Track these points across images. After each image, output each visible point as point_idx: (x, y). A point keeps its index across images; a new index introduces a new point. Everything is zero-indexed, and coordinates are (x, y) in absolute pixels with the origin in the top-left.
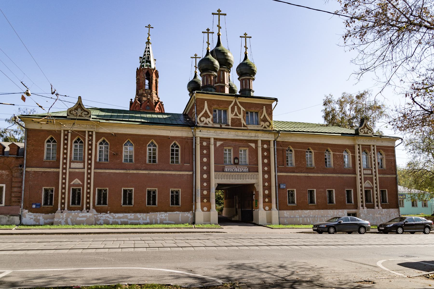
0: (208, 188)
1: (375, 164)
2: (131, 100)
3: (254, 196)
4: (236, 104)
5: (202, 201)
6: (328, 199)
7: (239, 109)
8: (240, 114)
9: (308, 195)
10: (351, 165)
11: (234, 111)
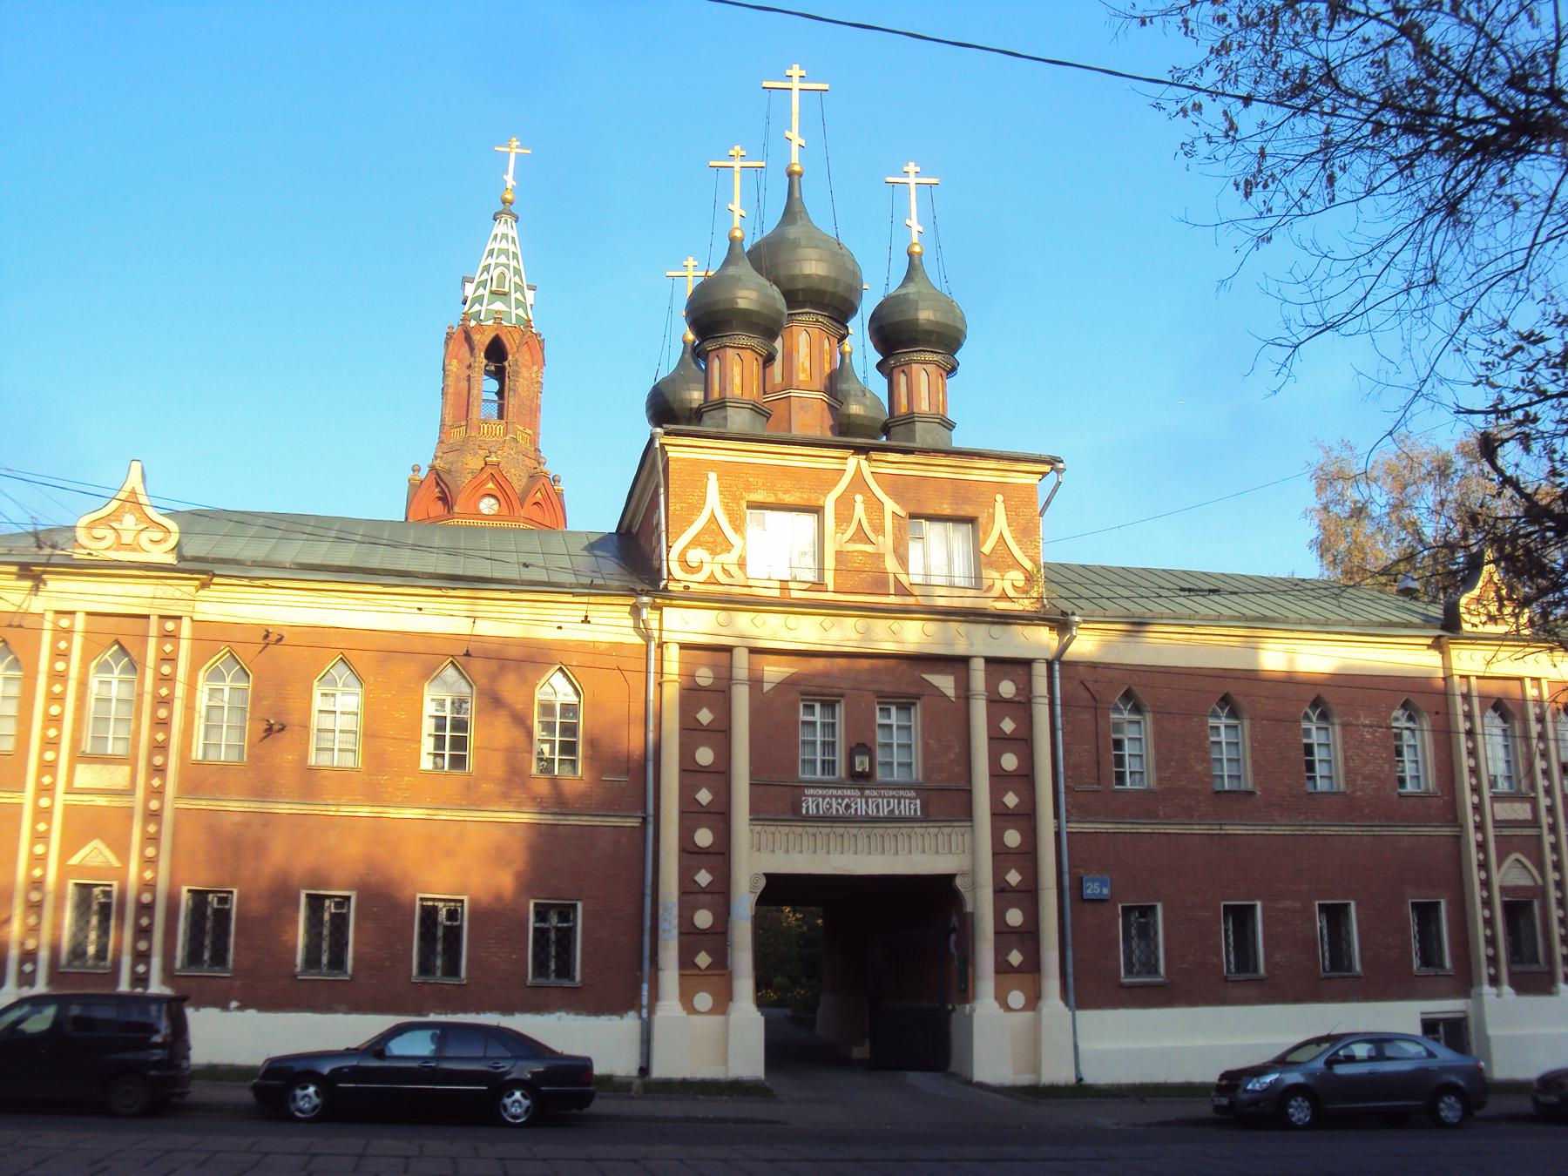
0: (721, 895)
1: (1546, 773)
2: (416, 469)
3: (953, 937)
4: (858, 482)
5: (686, 962)
6: (1324, 953)
7: (875, 506)
8: (879, 530)
9: (1224, 933)
11: (849, 520)
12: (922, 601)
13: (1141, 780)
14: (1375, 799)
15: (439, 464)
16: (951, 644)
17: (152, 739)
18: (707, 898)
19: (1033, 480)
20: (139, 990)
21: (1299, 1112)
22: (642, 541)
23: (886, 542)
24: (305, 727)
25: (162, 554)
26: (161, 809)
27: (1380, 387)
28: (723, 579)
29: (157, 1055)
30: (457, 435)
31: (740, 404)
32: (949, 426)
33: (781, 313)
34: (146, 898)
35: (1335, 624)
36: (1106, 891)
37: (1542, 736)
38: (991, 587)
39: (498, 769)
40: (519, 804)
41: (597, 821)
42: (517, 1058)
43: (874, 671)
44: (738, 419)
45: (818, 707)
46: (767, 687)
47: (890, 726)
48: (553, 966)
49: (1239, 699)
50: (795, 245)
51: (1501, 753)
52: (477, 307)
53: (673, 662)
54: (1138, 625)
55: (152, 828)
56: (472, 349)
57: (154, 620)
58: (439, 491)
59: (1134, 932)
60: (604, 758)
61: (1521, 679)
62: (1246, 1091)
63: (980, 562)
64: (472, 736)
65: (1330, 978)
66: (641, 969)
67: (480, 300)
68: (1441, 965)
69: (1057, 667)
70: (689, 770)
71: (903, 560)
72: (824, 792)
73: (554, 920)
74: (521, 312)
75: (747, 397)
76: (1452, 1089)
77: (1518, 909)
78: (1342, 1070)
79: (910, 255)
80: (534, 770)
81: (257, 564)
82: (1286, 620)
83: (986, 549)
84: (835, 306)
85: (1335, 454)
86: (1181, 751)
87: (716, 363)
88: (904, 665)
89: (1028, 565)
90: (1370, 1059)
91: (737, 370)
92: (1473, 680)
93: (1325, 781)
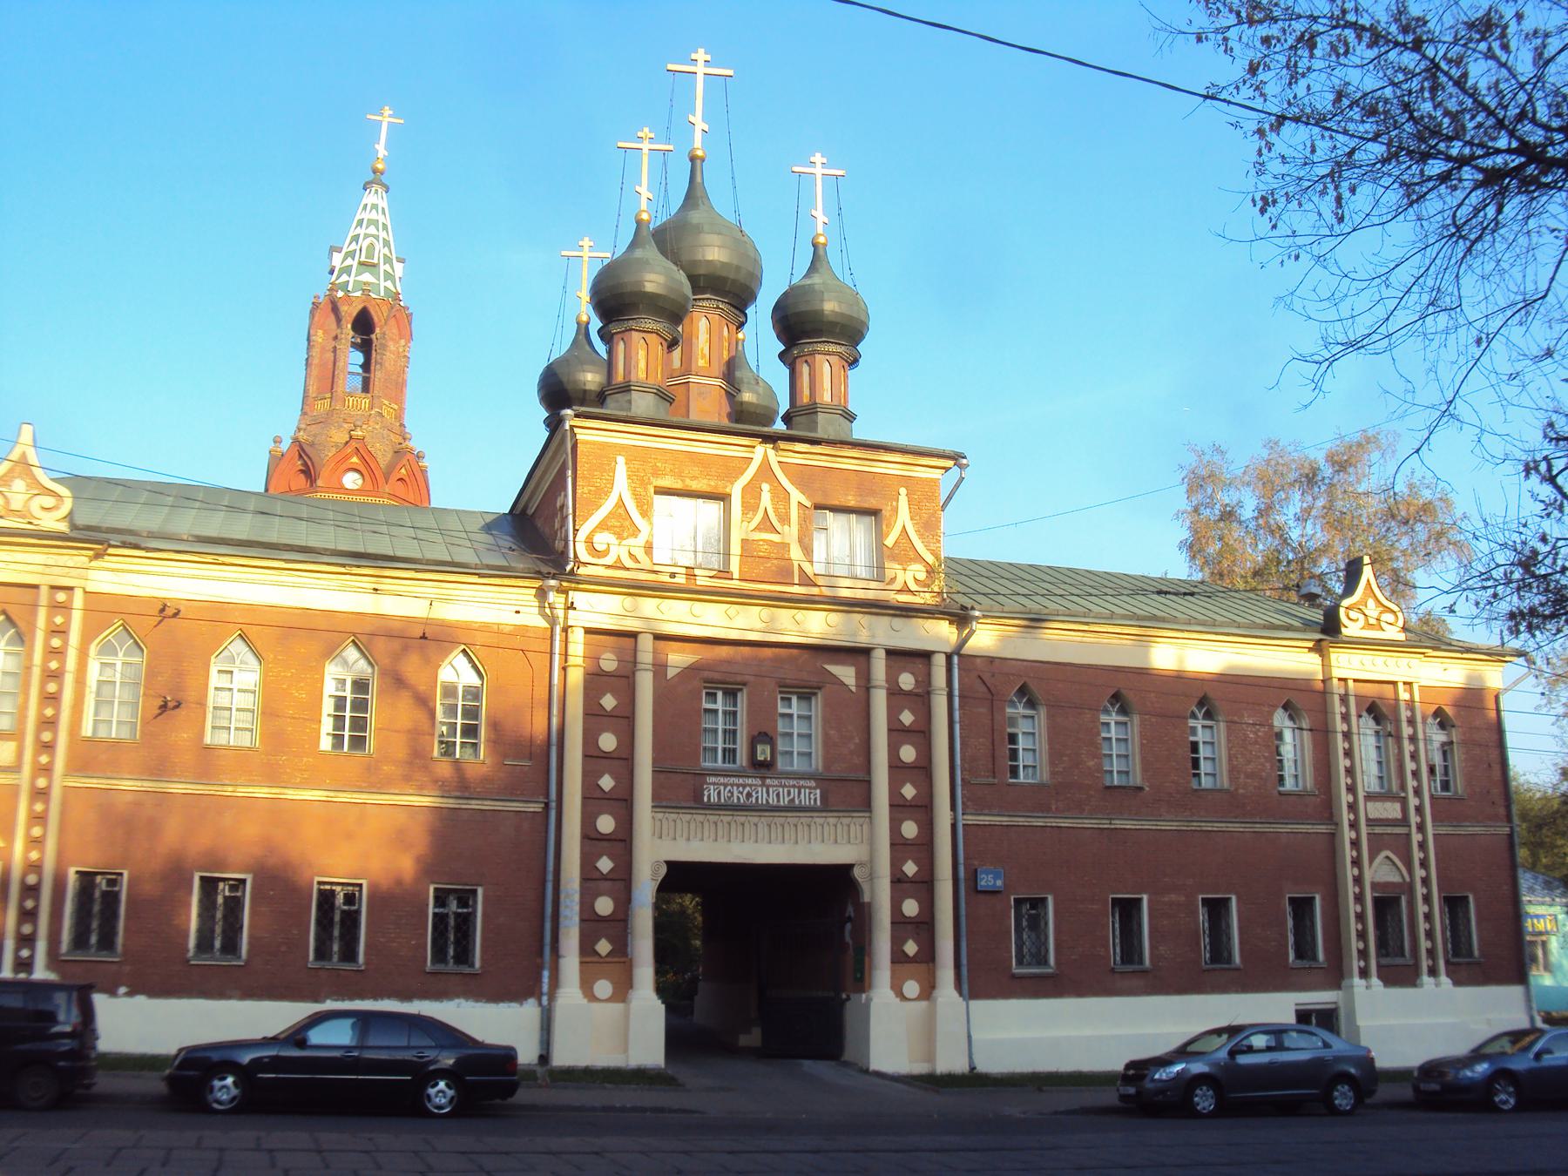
0: (623, 880)
1: (1416, 774)
2: (277, 441)
3: (848, 926)
4: (765, 471)
5: (587, 948)
6: (1205, 941)
7: (781, 496)
8: (785, 519)
9: (1113, 925)
10: (1309, 782)
11: (755, 509)
12: (827, 592)
13: (1034, 774)
14: (1258, 795)
15: (302, 436)
16: (855, 635)
17: (40, 714)
18: (607, 884)
19: (936, 474)
20: (22, 976)
21: (1204, 1100)
22: (539, 523)
23: (791, 532)
24: (202, 704)
25: (53, 522)
26: (49, 787)
27: (1406, 406)
28: (629, 563)
29: (66, 1045)
30: (321, 407)
31: (644, 389)
32: (850, 417)
33: (687, 298)
34: (32, 879)
35: (1222, 625)
36: (999, 883)
37: (1413, 739)
38: (893, 580)
39: (401, 753)
40: (421, 787)
41: (498, 806)
42: (442, 1047)
43: (776, 659)
44: (643, 404)
45: (720, 695)
46: (671, 673)
47: (791, 716)
48: (451, 952)
49: (1130, 696)
50: (698, 229)
51: (1373, 754)
52: (344, 278)
53: (578, 645)
54: (1035, 621)
55: (39, 807)
56: (339, 320)
57: (44, 591)
58: (302, 465)
59: (1025, 923)
60: (507, 742)
61: (1394, 683)
62: (1153, 1080)
63: (881, 556)
64: (372, 717)
65: (1209, 969)
66: (541, 953)
67: (347, 270)
68: (1314, 958)
69: (956, 659)
70: (593, 756)
71: (808, 551)
72: (726, 780)
73: (453, 906)
74: (389, 284)
75: (651, 381)
76: (1345, 1077)
77: (1387, 904)
78: (1243, 1060)
79: (815, 245)
80: (436, 753)
81: (152, 535)
82: (1175, 620)
83: (889, 542)
84: (734, 293)
85: (1207, 458)
86: (1072, 743)
87: (621, 346)
88: (806, 655)
89: (930, 559)
90: (1269, 1049)
91: (642, 354)
92: (1350, 683)
93: (1210, 779)
